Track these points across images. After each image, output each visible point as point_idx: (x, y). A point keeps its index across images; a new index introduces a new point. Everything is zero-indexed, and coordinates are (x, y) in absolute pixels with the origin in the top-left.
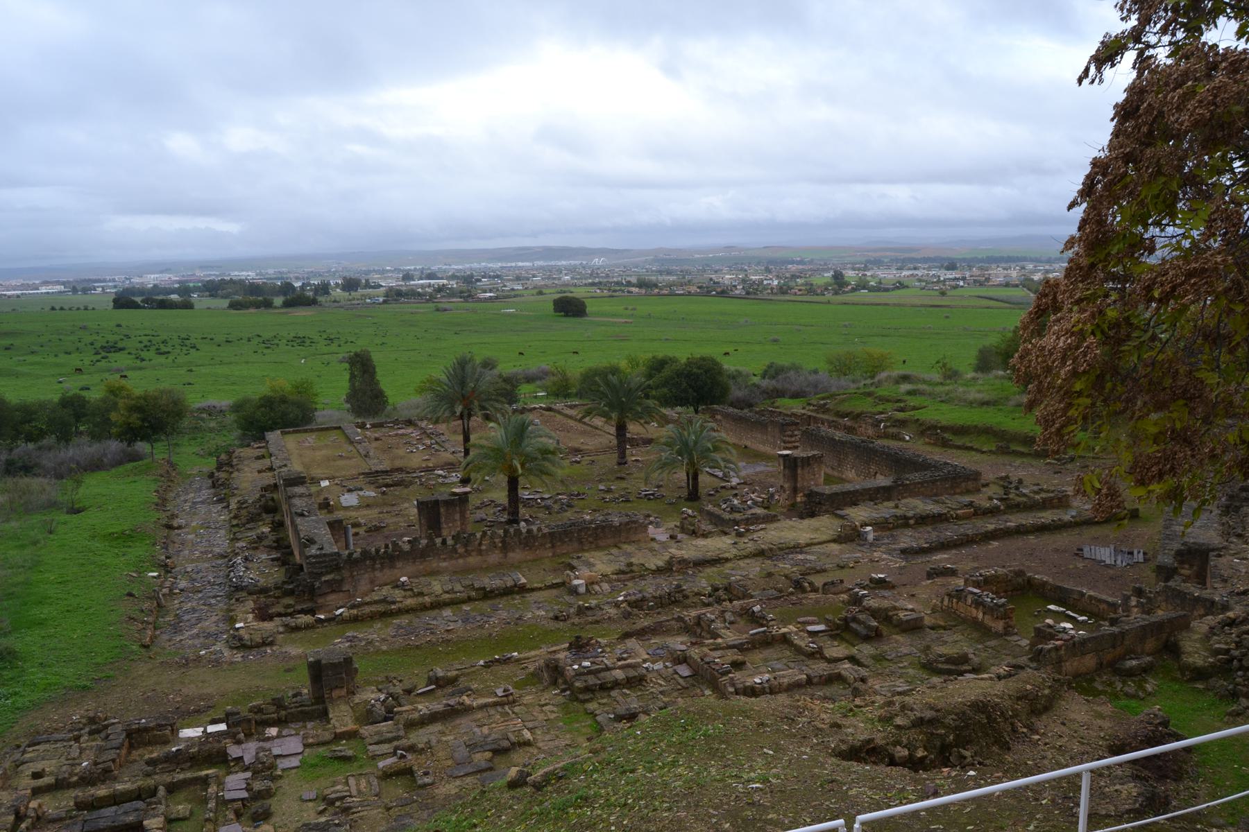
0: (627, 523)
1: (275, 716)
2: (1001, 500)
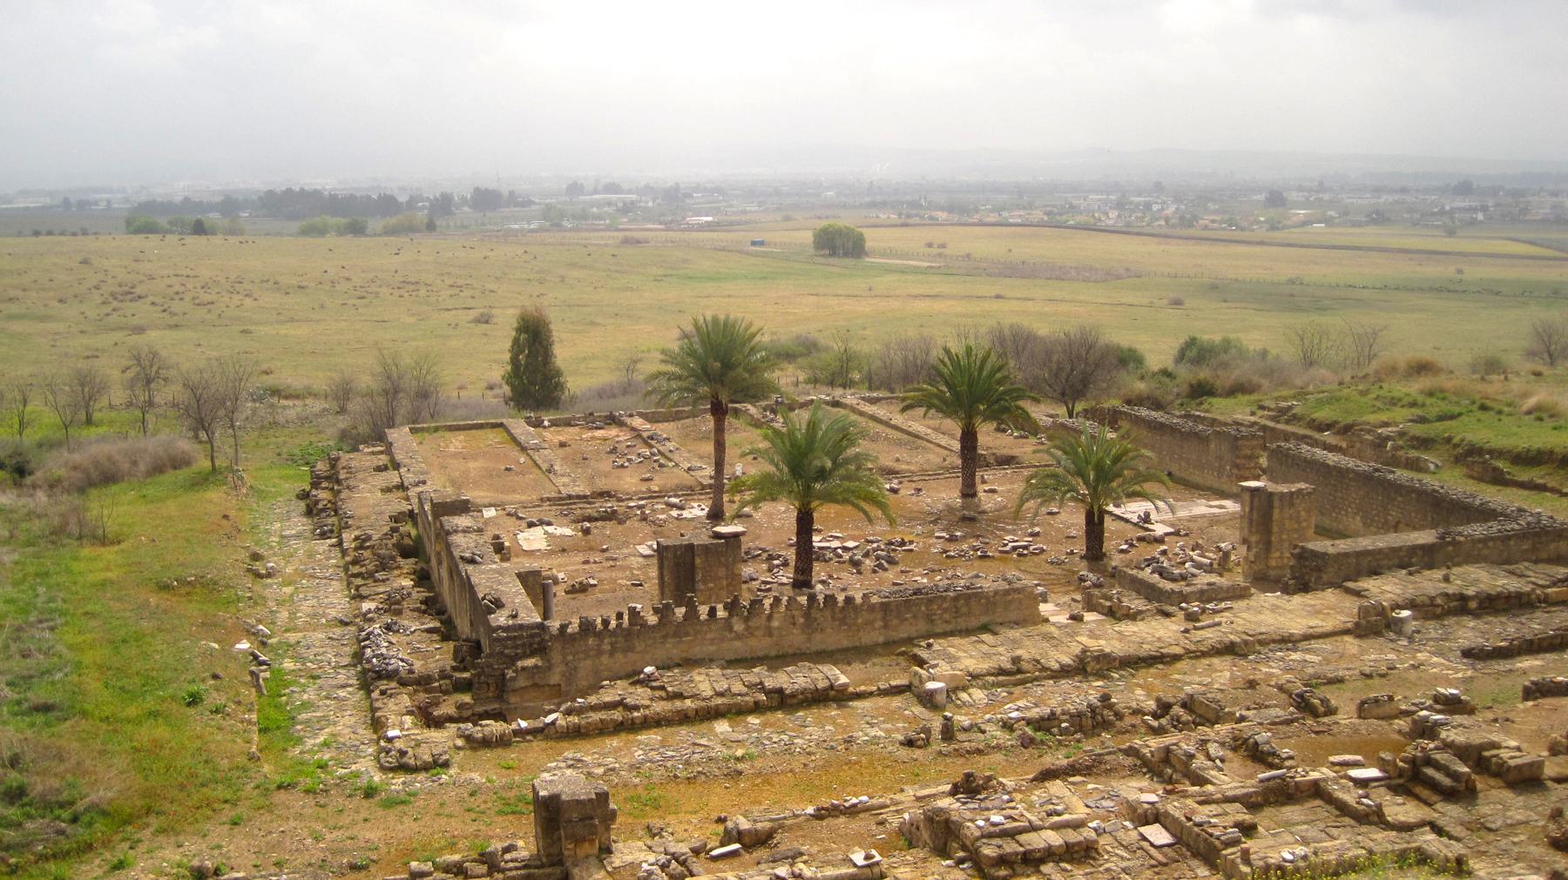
0: (1007, 592)
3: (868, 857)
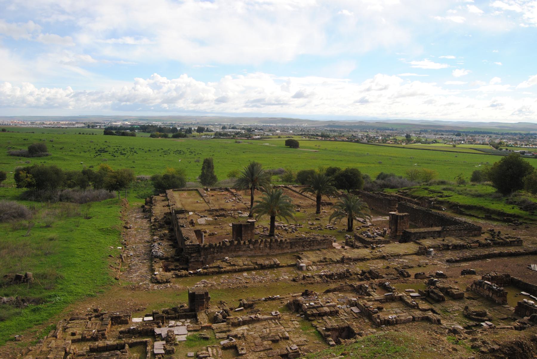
1: (174, 315)
2: (491, 240)
3: (276, 313)
